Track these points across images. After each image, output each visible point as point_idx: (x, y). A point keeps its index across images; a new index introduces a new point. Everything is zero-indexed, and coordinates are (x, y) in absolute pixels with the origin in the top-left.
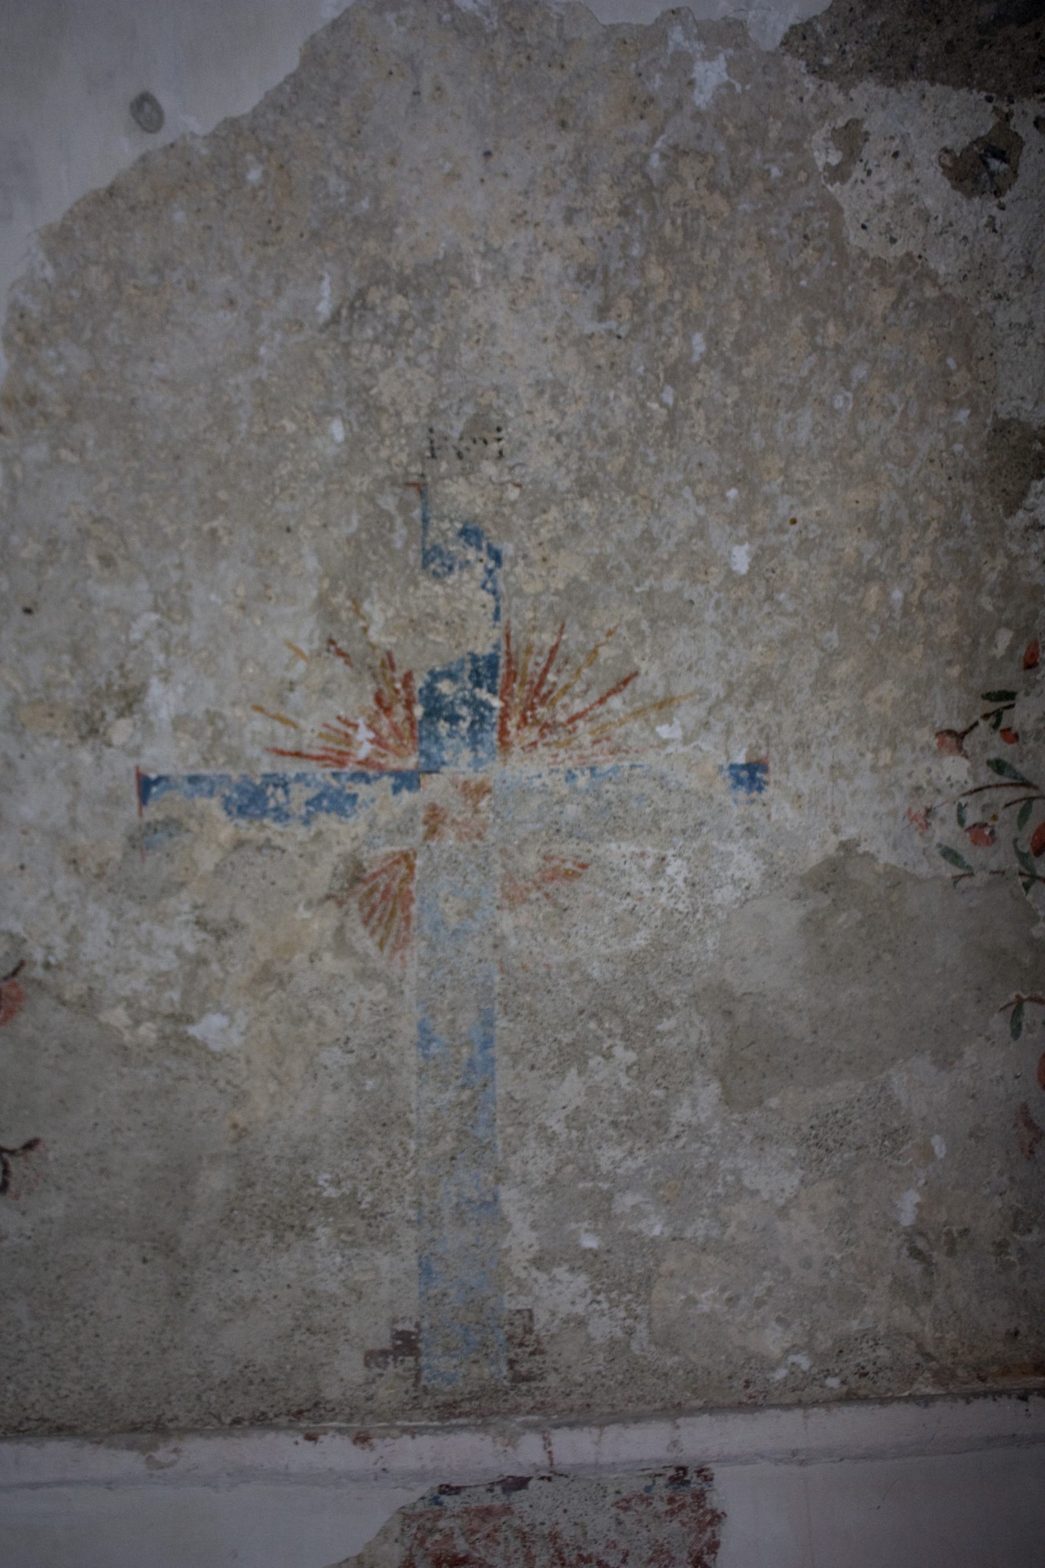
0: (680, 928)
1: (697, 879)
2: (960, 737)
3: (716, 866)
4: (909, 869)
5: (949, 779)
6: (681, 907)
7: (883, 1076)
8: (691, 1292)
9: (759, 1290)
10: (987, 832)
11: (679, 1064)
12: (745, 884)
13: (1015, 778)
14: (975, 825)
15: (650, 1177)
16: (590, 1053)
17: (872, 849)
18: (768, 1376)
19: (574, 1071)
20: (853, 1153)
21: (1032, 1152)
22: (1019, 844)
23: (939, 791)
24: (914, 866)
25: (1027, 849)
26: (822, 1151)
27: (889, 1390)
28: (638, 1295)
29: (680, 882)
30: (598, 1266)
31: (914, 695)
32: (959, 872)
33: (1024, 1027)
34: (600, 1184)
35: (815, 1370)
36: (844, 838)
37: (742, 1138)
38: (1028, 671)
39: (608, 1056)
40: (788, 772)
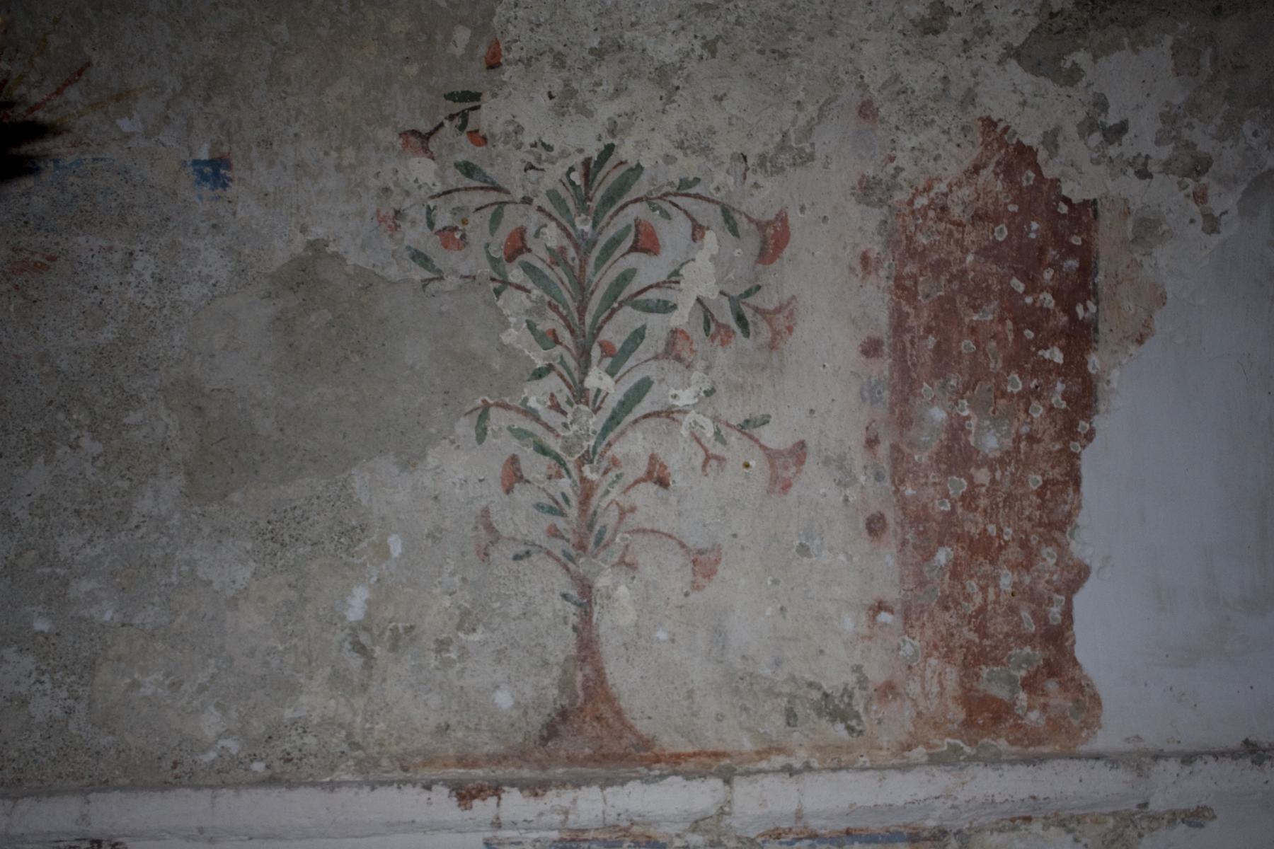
0: (148, 322)
1: (164, 275)
2: (426, 137)
3: (183, 262)
4: (377, 271)
5: (416, 181)
6: (148, 302)
7: (344, 476)
8: (136, 676)
9: (203, 678)
10: (457, 236)
11: (144, 457)
12: (212, 281)
13: (485, 181)
14: (445, 229)
15: (107, 564)
16: (58, 444)
17: (341, 250)
18: (196, 758)
19: (41, 460)
20: (309, 548)
21: (486, 555)
22: (492, 249)
23: (408, 193)
24: (383, 268)
25: (499, 254)
26: (277, 546)
27: (311, 775)
28: (81, 677)
29: (147, 277)
30: (46, 649)
31: (373, 93)
32: (428, 275)
33: (489, 432)
34: (58, 570)
35: (242, 755)
36: (311, 238)
37: (199, 529)
38: (492, 71)
39: (75, 447)
40: (251, 169)
